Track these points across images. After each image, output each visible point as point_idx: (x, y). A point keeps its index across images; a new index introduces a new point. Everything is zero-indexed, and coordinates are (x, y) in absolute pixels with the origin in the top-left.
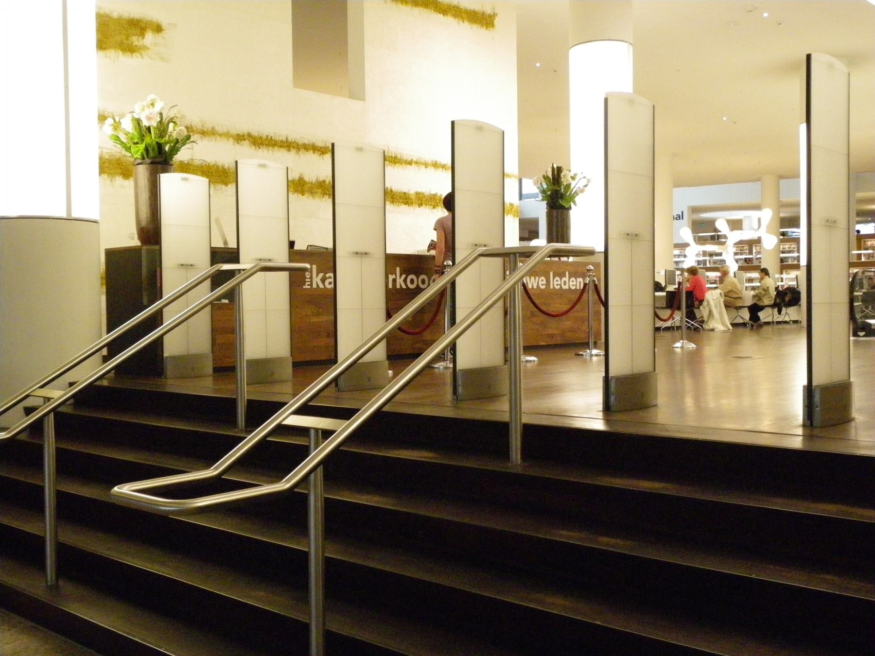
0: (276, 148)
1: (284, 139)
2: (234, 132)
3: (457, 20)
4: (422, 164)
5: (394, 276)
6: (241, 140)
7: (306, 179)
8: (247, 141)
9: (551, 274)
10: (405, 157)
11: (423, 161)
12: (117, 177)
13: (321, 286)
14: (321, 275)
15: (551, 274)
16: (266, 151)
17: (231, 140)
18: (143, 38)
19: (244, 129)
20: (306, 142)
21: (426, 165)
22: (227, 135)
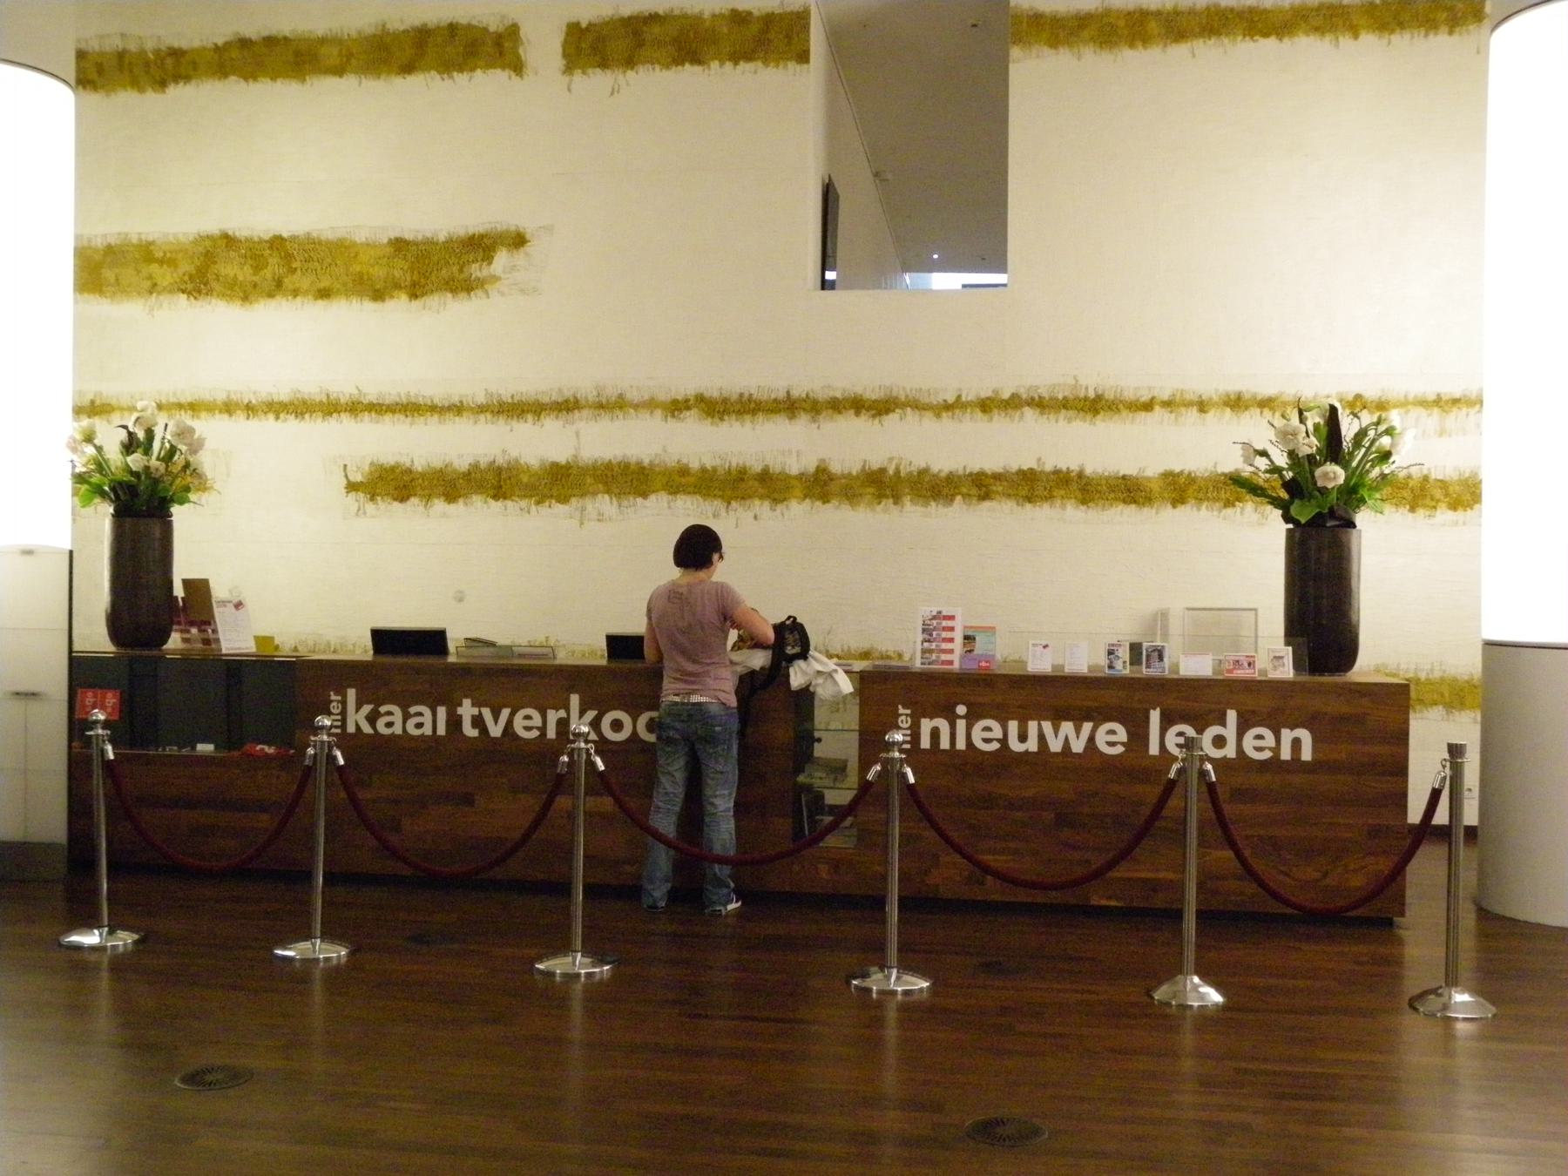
0: (760, 417)
1: (782, 395)
2: (663, 396)
3: (1328, 37)
4: (1189, 404)
5: (562, 713)
6: (680, 410)
7: (836, 468)
8: (694, 412)
9: (1155, 716)
10: (1129, 395)
11: (1189, 397)
12: (436, 501)
13: (367, 729)
14: (367, 709)
15: (1155, 716)
16: (737, 425)
17: (659, 413)
18: (490, 263)
19: (686, 386)
20: (838, 395)
21: (1202, 406)
22: (650, 405)
